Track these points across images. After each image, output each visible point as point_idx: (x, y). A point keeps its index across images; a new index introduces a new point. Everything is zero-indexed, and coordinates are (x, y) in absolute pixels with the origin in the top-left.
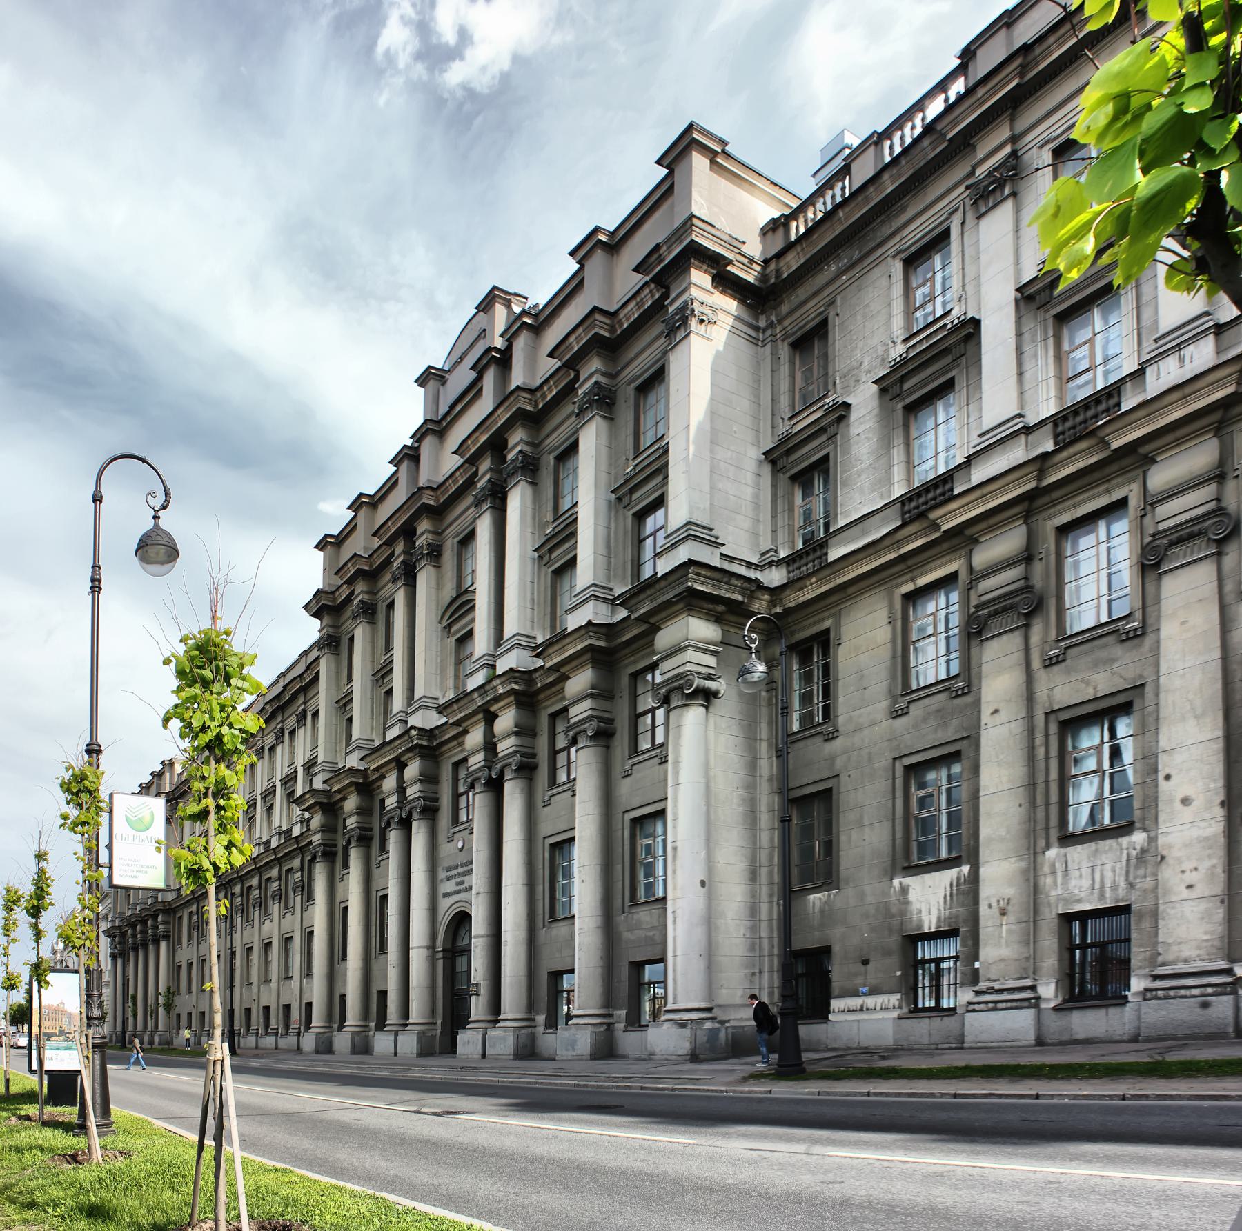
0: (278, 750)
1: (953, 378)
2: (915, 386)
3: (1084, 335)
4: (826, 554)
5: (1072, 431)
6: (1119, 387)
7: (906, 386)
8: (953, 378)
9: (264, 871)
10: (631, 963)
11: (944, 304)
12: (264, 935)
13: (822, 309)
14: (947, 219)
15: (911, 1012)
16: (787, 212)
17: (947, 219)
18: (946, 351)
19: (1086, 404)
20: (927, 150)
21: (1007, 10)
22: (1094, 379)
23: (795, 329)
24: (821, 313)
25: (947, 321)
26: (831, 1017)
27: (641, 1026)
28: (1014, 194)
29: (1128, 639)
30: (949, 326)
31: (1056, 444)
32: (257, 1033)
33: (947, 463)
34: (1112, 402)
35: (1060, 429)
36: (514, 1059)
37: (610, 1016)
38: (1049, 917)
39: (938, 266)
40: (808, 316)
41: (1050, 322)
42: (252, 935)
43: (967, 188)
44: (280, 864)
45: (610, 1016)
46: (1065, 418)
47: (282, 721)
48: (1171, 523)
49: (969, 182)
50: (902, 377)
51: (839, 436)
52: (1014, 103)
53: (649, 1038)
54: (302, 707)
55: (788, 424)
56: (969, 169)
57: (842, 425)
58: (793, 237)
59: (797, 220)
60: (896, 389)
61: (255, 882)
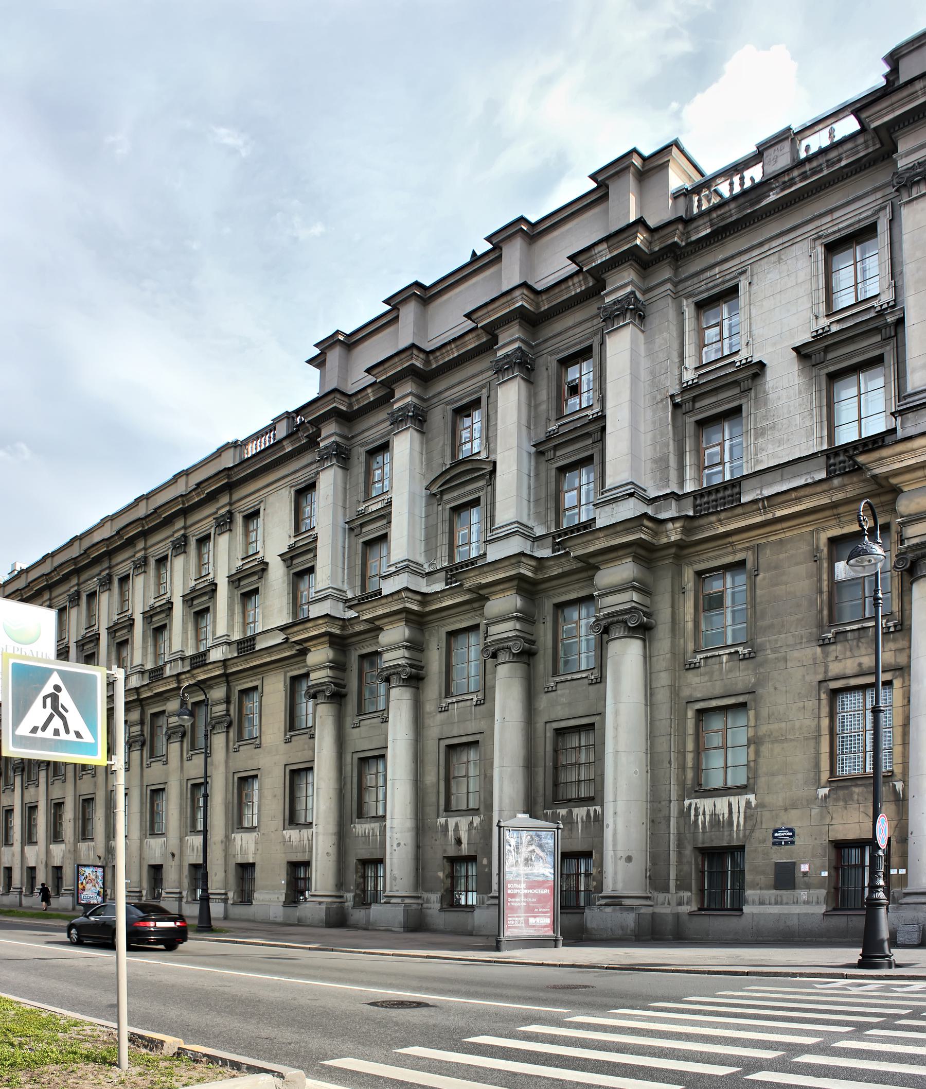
0: (104, 598)
1: (258, 588)
2: (709, 406)
3: (717, 439)
4: (254, 645)
5: (714, 503)
6: (884, 437)
7: (830, 356)
8: (258, 588)
9: (148, 704)
10: (190, 865)
11: (731, 346)
12: (27, 799)
13: (313, 475)
14: (259, 504)
15: (700, 909)
16: (689, 186)
17: (259, 504)
18: (736, 383)
19: (717, 489)
20: (860, 148)
21: (183, 471)
22: (723, 472)
23: (830, 231)
24: (312, 478)
25: (875, 303)
26: (746, 909)
27: (364, 904)
28: (230, 530)
29: (744, 659)
30: (738, 364)
31: (695, 512)
32: (21, 893)
33: (732, 472)
34: (736, 490)
35: (698, 502)
36: (404, 931)
37: (341, 897)
38: (352, 862)
39: (726, 315)
40: (716, 278)
41: (824, 379)
42: (37, 794)
43: (214, 519)
44: (228, 683)
45: (341, 897)
46: (702, 496)
47: (110, 568)
48: (218, 714)
49: (215, 516)
50: (827, 347)
51: (753, 391)
52: (230, 487)
53: (476, 919)
54: (76, 588)
55: (240, 563)
56: (171, 533)
57: (758, 382)
58: (695, 211)
59: (699, 194)
60: (237, 583)
61: (218, 693)
